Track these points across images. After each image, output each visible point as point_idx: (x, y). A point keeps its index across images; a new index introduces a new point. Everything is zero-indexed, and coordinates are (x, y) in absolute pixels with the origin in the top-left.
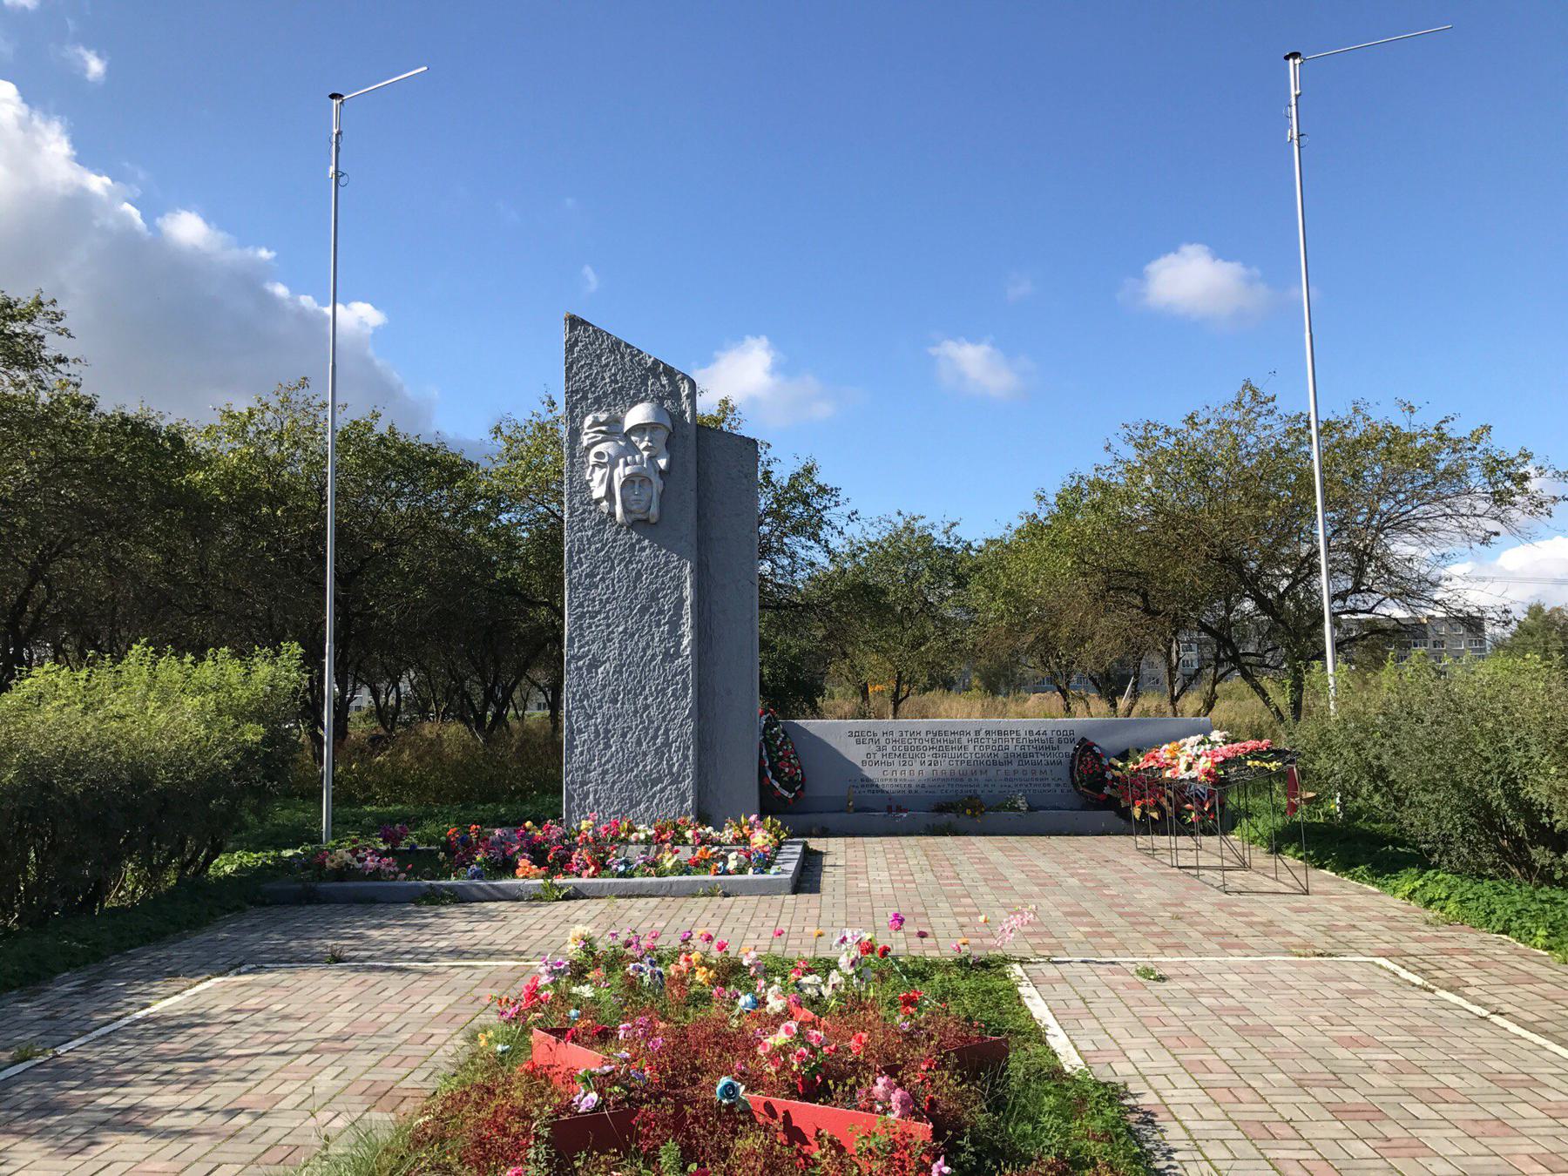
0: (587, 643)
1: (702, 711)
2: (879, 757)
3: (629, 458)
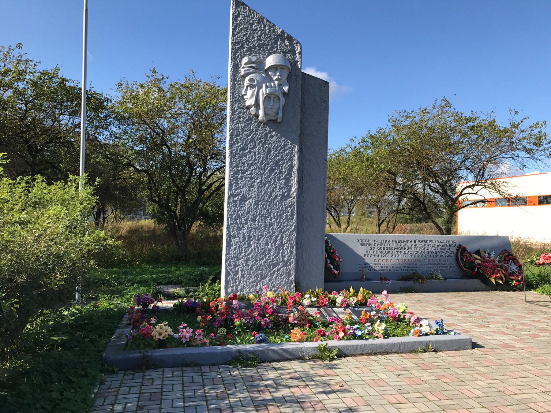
0: (240, 187)
1: (299, 229)
2: (372, 253)
3: (268, 84)
